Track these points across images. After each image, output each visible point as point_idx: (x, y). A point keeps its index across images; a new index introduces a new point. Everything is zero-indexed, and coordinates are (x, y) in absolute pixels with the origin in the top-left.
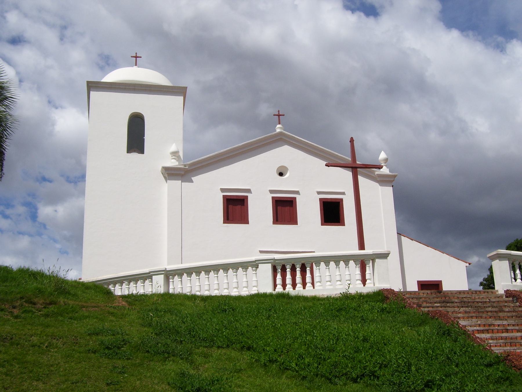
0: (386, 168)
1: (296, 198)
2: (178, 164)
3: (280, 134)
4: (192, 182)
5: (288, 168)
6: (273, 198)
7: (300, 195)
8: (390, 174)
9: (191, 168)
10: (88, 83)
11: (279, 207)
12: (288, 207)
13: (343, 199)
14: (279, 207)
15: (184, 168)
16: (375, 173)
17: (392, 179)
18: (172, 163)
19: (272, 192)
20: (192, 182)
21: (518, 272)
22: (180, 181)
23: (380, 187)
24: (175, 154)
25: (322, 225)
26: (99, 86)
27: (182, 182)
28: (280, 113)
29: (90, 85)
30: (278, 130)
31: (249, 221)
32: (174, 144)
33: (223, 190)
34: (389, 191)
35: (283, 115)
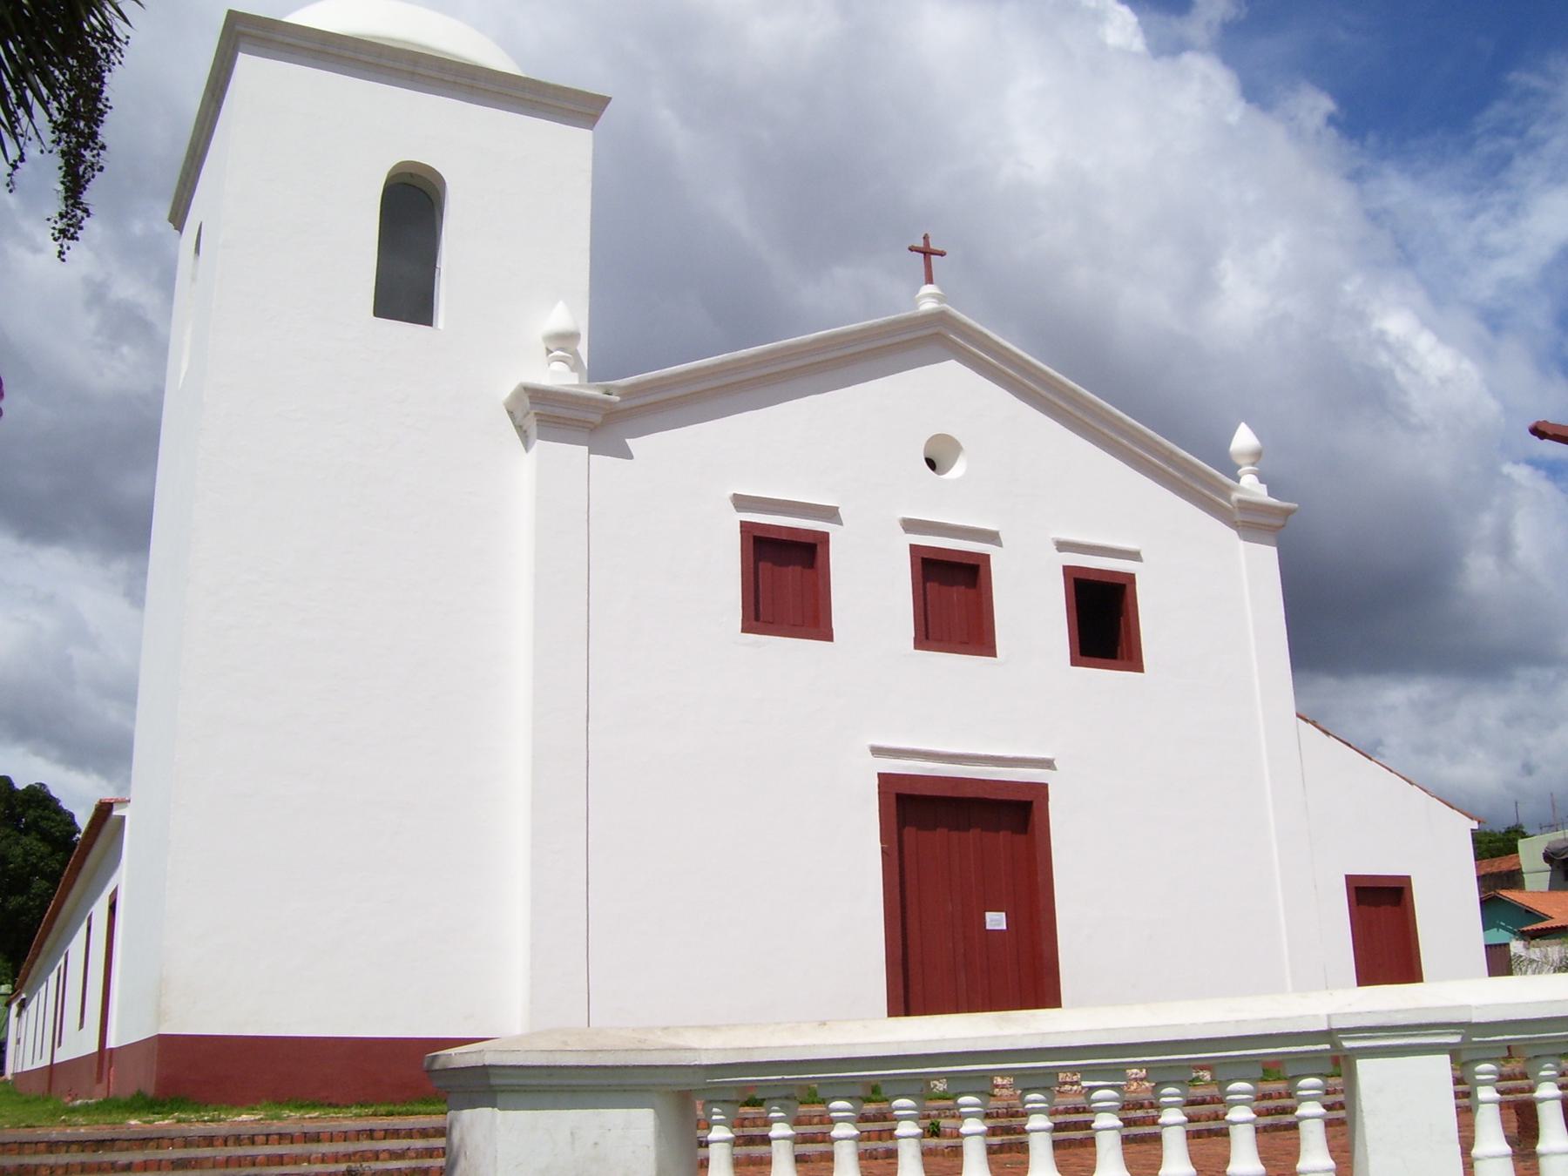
0: (1257, 482)
1: (988, 556)
2: (577, 382)
3: (940, 318)
4: (627, 455)
5: (962, 444)
6: (745, 526)
7: (841, 524)
8: (1273, 501)
9: (627, 405)
10: (234, 18)
11: (761, 565)
12: (798, 568)
13: (1133, 575)
14: (761, 565)
15: (605, 402)
16: (1230, 496)
17: (1278, 522)
18: (559, 376)
19: (910, 526)
20: (627, 455)
21: (343, 1167)
22: (586, 448)
23: (1242, 542)
24: (564, 340)
25: (1074, 663)
26: (280, 38)
27: (589, 453)
28: (933, 246)
29: (239, 28)
30: (928, 306)
31: (831, 630)
32: (561, 302)
33: (741, 502)
34: (1268, 556)
35: (942, 254)
